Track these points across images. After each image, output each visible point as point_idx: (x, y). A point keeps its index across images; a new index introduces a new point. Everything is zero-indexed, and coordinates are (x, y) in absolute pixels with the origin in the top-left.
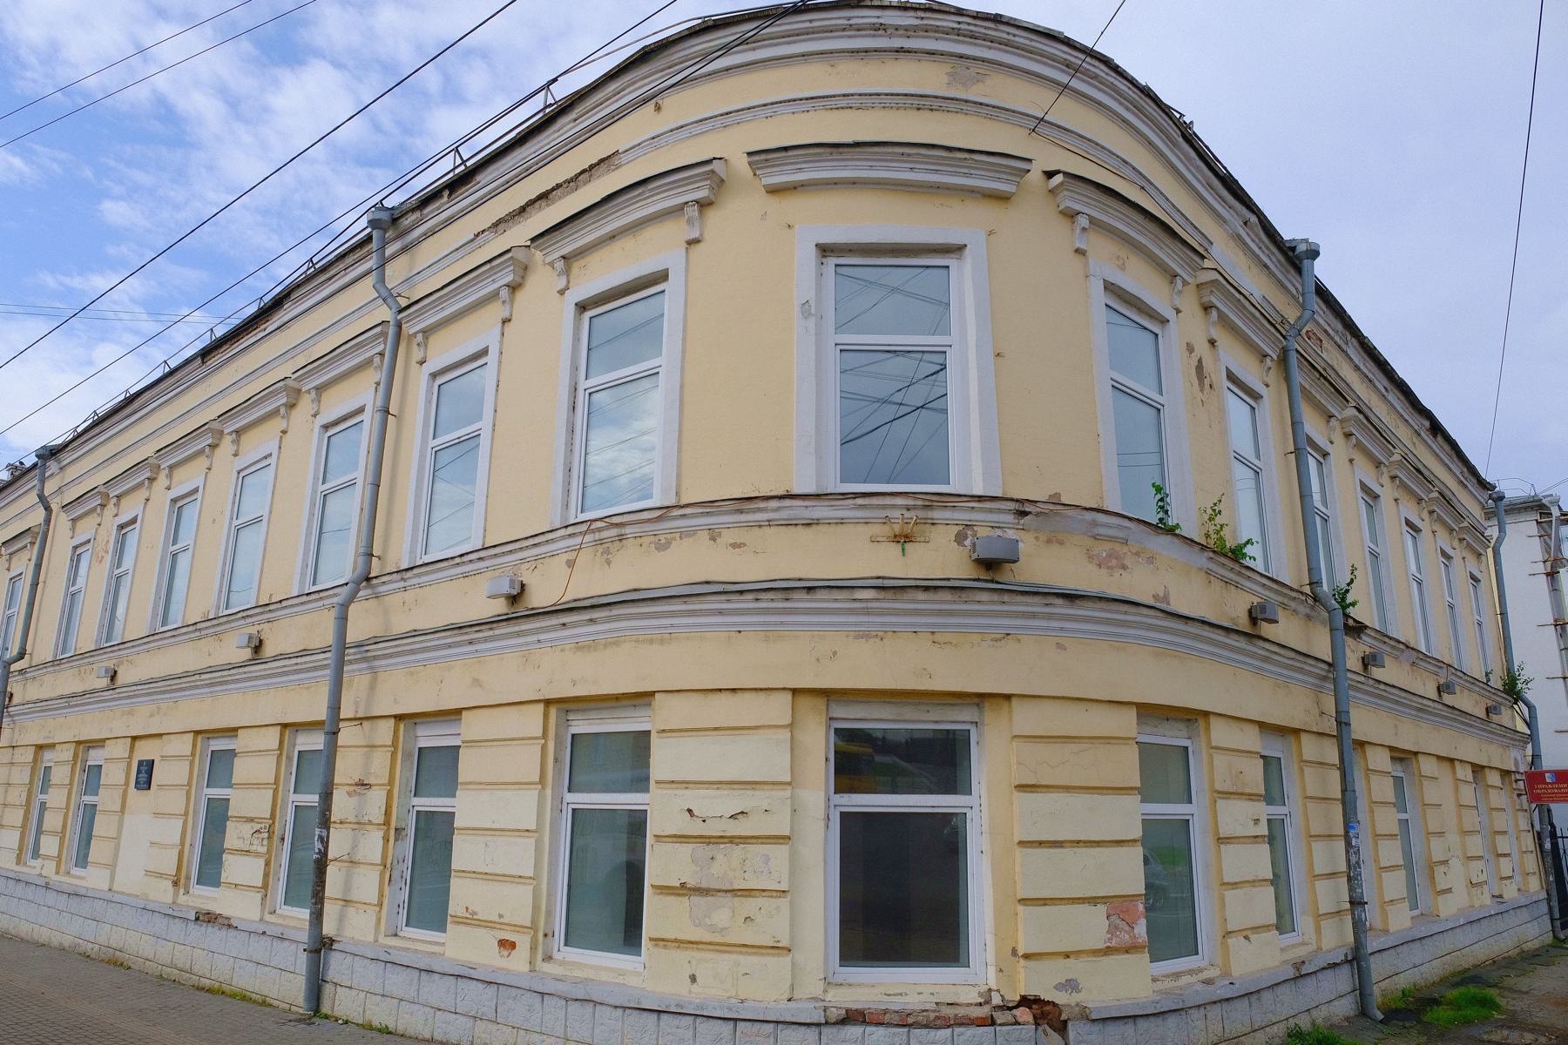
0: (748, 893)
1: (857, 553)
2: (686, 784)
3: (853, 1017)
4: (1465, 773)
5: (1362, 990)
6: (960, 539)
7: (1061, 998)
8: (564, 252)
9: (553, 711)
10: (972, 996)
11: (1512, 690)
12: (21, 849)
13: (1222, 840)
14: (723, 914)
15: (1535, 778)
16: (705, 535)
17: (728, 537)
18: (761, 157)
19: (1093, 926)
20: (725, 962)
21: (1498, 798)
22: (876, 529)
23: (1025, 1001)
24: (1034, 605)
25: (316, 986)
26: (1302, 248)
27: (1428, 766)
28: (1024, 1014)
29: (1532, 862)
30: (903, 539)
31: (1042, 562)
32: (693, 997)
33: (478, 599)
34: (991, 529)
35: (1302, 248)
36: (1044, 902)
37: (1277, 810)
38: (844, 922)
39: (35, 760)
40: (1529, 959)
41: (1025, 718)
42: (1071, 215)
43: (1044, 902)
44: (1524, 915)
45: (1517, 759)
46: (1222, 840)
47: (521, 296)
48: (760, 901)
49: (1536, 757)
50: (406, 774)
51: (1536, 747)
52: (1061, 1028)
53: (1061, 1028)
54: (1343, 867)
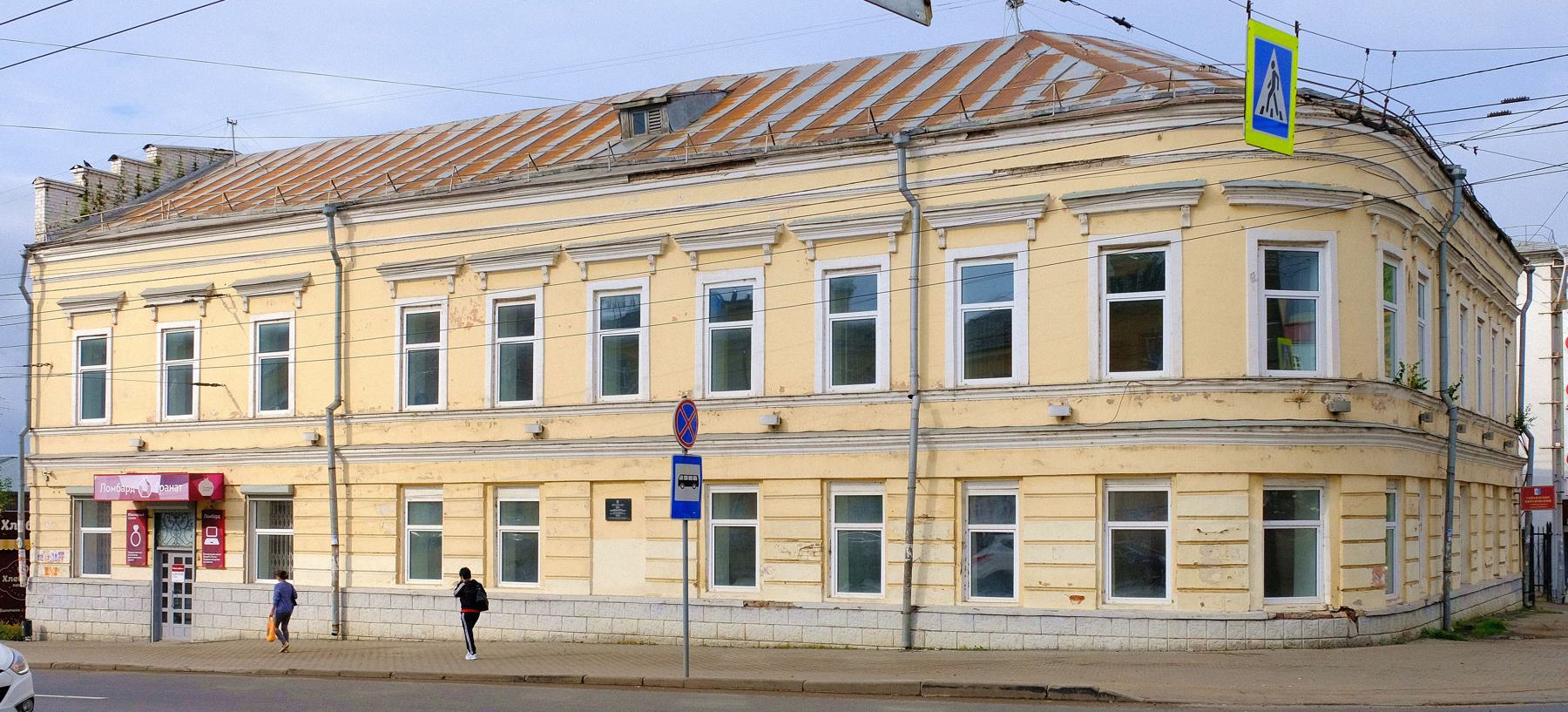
0: (1228, 566)
1: (1276, 407)
2: (1195, 517)
3: (1279, 616)
4: (1489, 492)
5: (1445, 618)
6: (1323, 400)
7: (1355, 608)
8: (1090, 210)
9: (1100, 481)
10: (1321, 608)
11: (1520, 426)
12: (398, 570)
13: (1406, 539)
14: (1216, 576)
15: (1527, 492)
16: (1201, 396)
17: (1214, 396)
18: (1232, 188)
19: (1366, 577)
20: (1219, 596)
21: (1504, 508)
22: (1286, 396)
23: (1342, 609)
24: (1355, 433)
25: (910, 631)
26: (1456, 171)
27: (1475, 490)
28: (1343, 614)
29: (1516, 553)
30: (1300, 400)
31: (1361, 412)
32: (1205, 612)
33: (1041, 414)
34: (1339, 394)
35: (1456, 171)
36: (1350, 567)
37: (1391, 524)
38: (1297, 573)
39: (398, 496)
40: (1516, 614)
41: (1347, 485)
42: (1372, 216)
43: (1350, 567)
44: (1509, 588)
45: (1515, 478)
46: (1406, 539)
47: (1041, 225)
48: (1236, 570)
49: (1529, 476)
50: (962, 510)
51: (1530, 467)
52: (1355, 620)
53: (1355, 620)
54: (1441, 553)
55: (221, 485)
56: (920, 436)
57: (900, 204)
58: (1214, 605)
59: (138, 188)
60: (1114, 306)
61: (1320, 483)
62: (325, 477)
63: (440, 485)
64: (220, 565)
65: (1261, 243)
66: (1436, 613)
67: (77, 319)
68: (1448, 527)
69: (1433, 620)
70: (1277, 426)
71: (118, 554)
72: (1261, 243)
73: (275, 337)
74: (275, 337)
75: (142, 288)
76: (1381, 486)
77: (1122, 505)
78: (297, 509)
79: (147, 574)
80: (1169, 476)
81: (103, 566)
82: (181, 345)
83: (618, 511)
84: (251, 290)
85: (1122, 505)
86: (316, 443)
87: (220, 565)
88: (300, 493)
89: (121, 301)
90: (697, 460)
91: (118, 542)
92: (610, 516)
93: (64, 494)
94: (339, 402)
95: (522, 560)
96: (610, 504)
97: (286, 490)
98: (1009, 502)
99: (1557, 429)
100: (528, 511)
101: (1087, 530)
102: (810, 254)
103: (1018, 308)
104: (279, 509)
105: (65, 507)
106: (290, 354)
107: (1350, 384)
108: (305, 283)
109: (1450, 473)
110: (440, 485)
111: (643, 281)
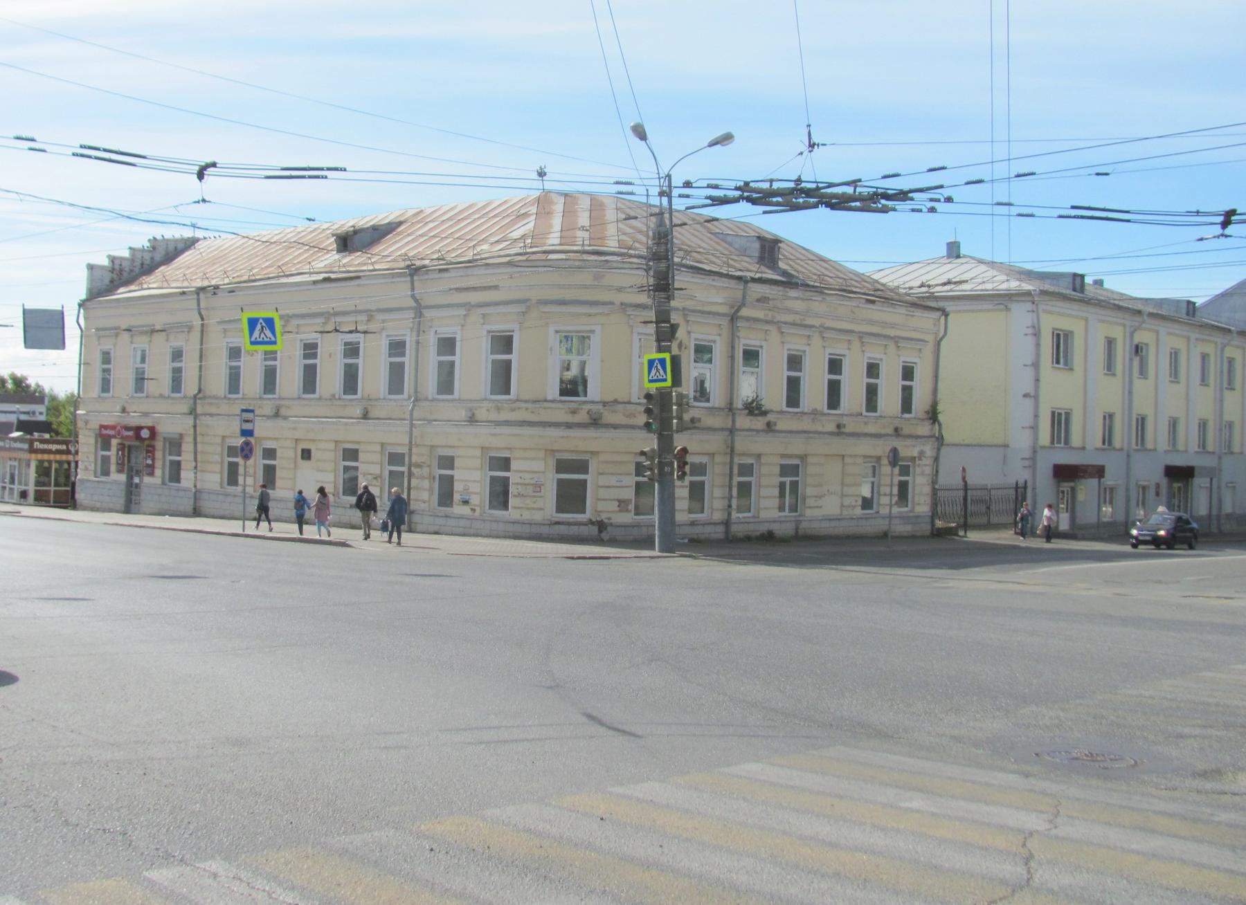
5: (727, 532)
55: (152, 430)
58: (527, 516)
60: (391, 363)
64: (152, 474)
66: (721, 529)
69: (718, 532)
71: (113, 468)
72: (489, 332)
77: (562, 466)
79: (123, 478)
81: (106, 472)
87: (152, 474)
91: (113, 460)
92: (303, 458)
94: (200, 391)
96: (303, 450)
99: (1242, 433)
101: (809, 480)
104: (175, 445)
106: (317, 361)
107: (605, 404)
111: (457, 329)
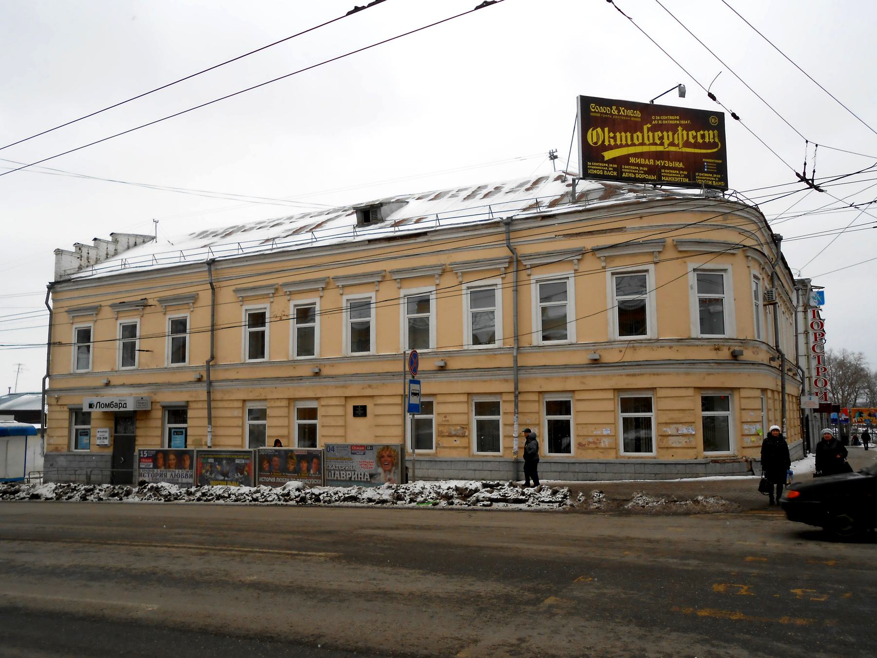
8: (606, 255)
33: (583, 358)
46: (538, 425)
56: (518, 369)
57: (504, 252)
59: (107, 254)
61: (729, 392)
62: (204, 397)
63: (265, 400)
65: (613, 274)
67: (121, 315)
68: (783, 416)
70: (706, 362)
73: (179, 326)
74: (179, 326)
75: (110, 303)
76: (758, 393)
78: (190, 413)
80: (653, 389)
82: (130, 331)
83: (360, 412)
84: (166, 303)
85: (627, 405)
86: (200, 380)
88: (192, 405)
89: (97, 309)
90: (418, 382)
92: (355, 415)
93: (66, 408)
95: (559, 435)
97: (183, 404)
98: (497, 404)
100: (311, 413)
102: (289, 298)
103: (373, 321)
105: (66, 415)
108: (194, 298)
109: (783, 388)
110: (265, 400)
